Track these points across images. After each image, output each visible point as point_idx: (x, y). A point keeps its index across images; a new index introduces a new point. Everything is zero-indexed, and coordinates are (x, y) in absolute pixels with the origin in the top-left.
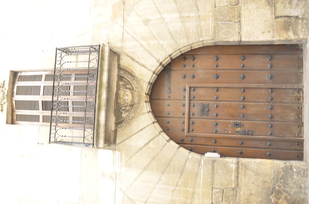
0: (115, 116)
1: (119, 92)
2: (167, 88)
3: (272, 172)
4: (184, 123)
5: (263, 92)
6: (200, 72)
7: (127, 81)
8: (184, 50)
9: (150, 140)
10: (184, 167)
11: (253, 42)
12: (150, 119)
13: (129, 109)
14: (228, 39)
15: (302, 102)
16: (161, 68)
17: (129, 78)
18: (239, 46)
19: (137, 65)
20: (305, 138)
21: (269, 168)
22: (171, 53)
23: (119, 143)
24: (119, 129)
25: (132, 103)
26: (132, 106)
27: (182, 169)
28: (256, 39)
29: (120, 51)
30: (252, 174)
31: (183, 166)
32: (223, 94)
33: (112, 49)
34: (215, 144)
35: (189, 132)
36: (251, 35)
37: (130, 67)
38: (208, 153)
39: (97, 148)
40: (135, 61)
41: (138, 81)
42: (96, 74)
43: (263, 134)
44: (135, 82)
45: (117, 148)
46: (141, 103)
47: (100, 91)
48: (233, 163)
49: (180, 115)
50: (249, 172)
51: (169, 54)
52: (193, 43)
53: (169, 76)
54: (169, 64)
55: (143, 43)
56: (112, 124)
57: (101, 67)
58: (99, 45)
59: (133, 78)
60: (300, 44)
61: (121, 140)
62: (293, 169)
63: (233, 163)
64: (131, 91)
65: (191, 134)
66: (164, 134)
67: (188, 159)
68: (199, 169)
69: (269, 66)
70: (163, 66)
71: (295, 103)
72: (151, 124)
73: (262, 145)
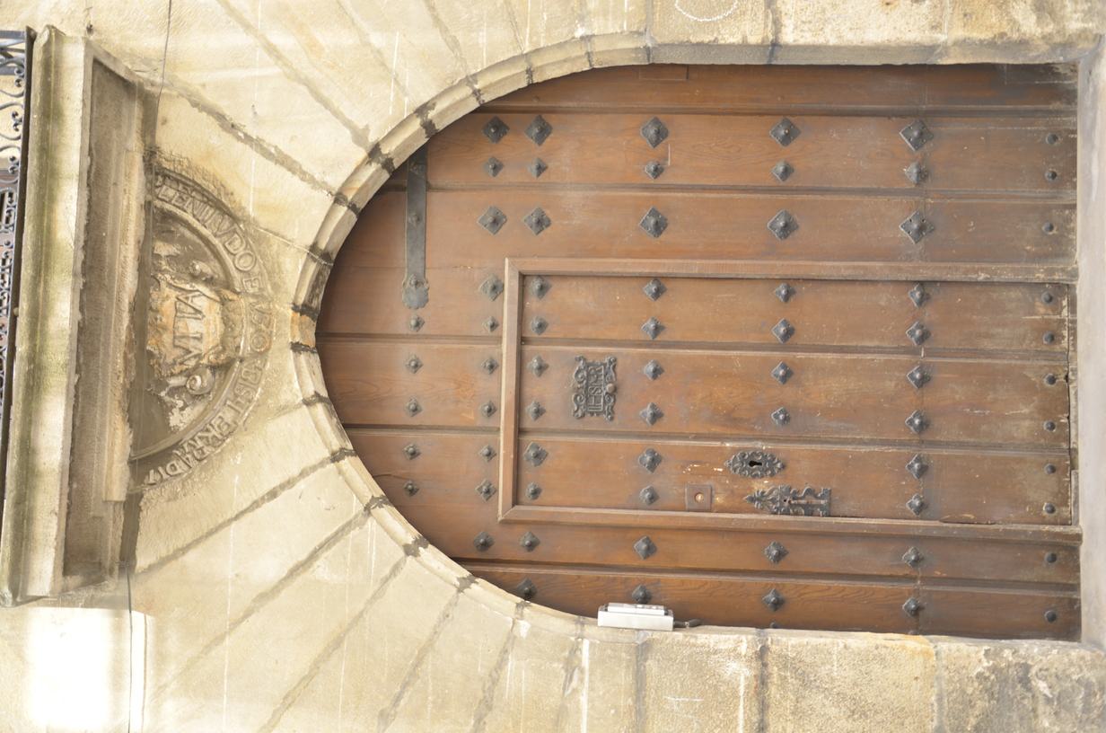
0: (131, 422)
1: (154, 295)
2: (407, 279)
3: (933, 698)
4: (491, 455)
5: (883, 303)
6: (573, 197)
7: (198, 241)
8: (491, 85)
9: (316, 544)
10: (495, 682)
11: (837, 48)
12: (318, 439)
13: (206, 384)
14: (713, 32)
15: (1071, 349)
16: (372, 176)
17: (205, 223)
18: (768, 69)
19: (254, 157)
20: (1083, 526)
21: (916, 678)
22: (425, 98)
23: (151, 568)
24: (150, 494)
25: (223, 357)
26: (221, 369)
27: (484, 691)
28: (851, 38)
29: (158, 80)
30: (833, 711)
31: (490, 675)
32: (684, 310)
33: (106, 62)
34: (649, 563)
35: (516, 501)
36: (828, 15)
37: (211, 167)
38: (613, 608)
39: (18, 599)
40: (241, 134)
41: (256, 240)
42: (16, 195)
43: (880, 505)
44: (238, 245)
45: (137, 594)
46: (270, 352)
47: (41, 290)
48: (738, 656)
49: (474, 416)
50: (816, 699)
51: (418, 105)
52: (537, 51)
53: (419, 220)
54: (420, 158)
55: (282, 40)
56: (110, 468)
57: (40, 158)
58: (29, 30)
59: (226, 224)
60: (1066, 64)
61: (164, 553)
62: (1033, 683)
63: (738, 656)
64: (218, 293)
65: (528, 511)
66: (389, 515)
67: (511, 638)
68: (570, 691)
69: (911, 171)
70: (387, 164)
71: (1038, 354)
72: (322, 464)
73: (878, 562)
